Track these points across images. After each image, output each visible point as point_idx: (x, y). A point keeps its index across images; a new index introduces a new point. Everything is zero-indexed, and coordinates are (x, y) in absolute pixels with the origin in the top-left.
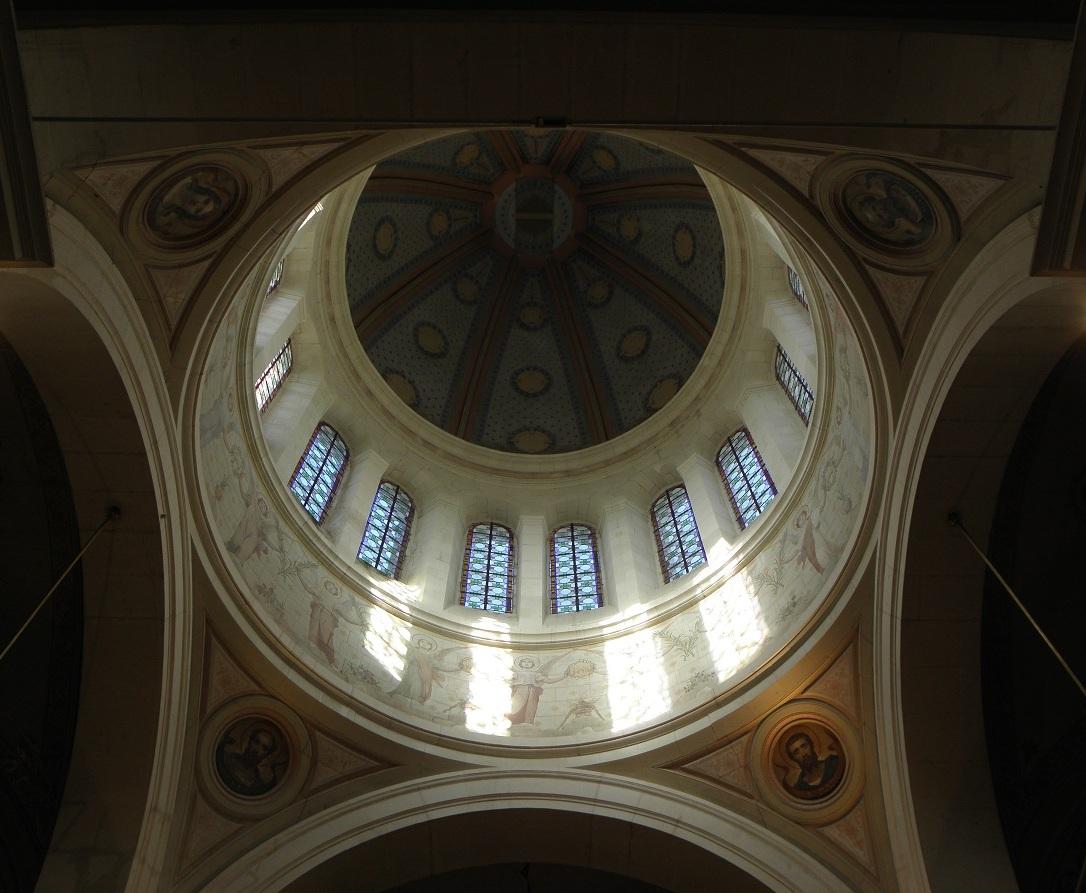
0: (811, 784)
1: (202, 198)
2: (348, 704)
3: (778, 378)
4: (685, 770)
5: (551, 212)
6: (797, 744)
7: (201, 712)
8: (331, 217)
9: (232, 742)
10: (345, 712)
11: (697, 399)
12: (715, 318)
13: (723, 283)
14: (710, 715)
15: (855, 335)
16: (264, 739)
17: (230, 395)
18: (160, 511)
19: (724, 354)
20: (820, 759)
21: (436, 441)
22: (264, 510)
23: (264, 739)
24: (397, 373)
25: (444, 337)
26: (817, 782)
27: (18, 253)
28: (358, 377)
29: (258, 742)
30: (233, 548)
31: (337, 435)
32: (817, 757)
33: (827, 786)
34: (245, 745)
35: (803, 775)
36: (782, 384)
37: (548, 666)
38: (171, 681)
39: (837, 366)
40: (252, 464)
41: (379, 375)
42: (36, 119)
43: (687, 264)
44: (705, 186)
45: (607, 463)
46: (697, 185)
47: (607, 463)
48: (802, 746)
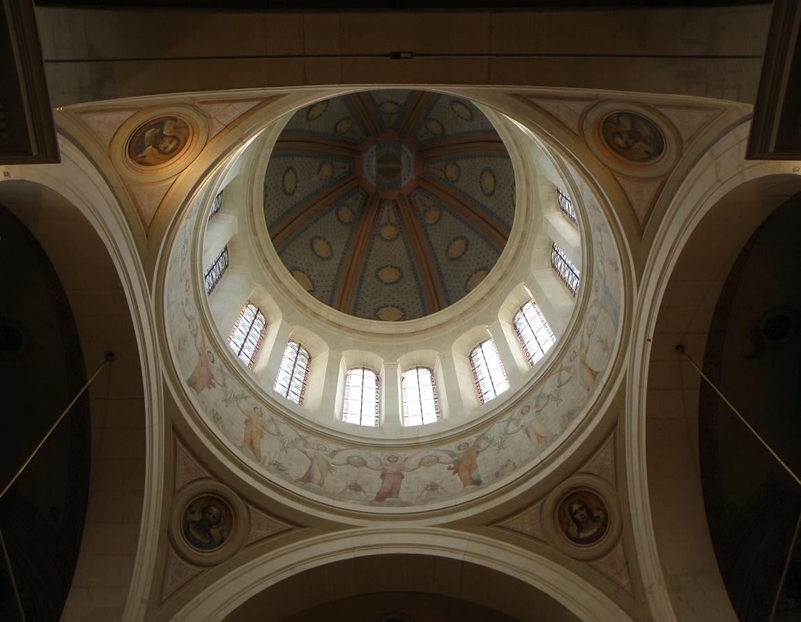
1: (578, 516)
3: (553, 266)
4: (583, 473)
5: (400, 163)
7: (171, 489)
8: (252, 157)
9: (646, 152)
12: (510, 229)
13: (514, 206)
14: (469, 510)
15: (613, 237)
18: (650, 345)
22: (212, 358)
23: (215, 510)
24: (299, 270)
26: (148, 134)
27: (35, 153)
30: (191, 383)
31: (259, 310)
33: (139, 135)
35: (162, 131)
36: (556, 269)
37: (335, 452)
39: (595, 253)
41: (287, 271)
42: (48, 61)
43: (491, 194)
44: (502, 142)
46: (504, 237)
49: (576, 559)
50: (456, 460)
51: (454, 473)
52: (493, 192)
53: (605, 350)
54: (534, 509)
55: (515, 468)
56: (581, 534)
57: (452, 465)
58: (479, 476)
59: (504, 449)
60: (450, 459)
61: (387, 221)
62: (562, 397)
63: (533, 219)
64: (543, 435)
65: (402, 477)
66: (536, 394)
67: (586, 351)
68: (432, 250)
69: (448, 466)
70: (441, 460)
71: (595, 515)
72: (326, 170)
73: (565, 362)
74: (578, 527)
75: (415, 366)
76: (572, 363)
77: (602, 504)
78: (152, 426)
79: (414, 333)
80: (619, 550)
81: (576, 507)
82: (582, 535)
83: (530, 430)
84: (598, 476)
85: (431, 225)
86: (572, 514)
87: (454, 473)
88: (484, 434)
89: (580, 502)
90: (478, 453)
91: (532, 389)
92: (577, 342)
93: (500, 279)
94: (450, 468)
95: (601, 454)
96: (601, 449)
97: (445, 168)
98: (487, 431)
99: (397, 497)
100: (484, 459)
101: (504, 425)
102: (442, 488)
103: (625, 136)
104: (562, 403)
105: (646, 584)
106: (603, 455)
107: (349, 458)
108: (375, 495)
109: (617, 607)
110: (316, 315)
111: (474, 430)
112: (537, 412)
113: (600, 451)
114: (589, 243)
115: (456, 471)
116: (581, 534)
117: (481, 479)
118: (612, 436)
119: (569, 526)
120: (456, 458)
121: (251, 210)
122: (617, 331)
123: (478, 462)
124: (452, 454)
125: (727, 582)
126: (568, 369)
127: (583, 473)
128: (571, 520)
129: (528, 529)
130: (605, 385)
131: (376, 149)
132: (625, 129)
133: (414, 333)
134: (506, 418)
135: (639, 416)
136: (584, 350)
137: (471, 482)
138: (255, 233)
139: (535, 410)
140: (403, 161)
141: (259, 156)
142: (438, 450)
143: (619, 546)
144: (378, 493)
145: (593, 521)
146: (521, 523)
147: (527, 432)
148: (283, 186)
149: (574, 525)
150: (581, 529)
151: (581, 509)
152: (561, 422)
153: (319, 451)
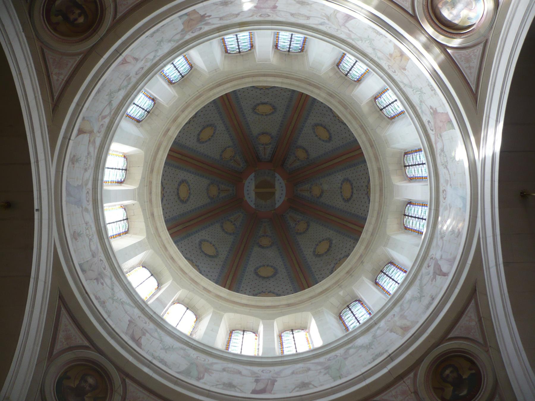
0: (460, 395)
1: (78, 11)
2: (148, 367)
4: (124, 382)
6: (448, 372)
9: (69, 378)
10: (146, 370)
11: (361, 256)
16: (91, 380)
17: (88, 192)
18: (36, 207)
19: (374, 229)
20: (464, 377)
21: (211, 289)
23: (91, 380)
25: (216, 249)
26: (464, 393)
28: (166, 249)
29: (86, 381)
32: (462, 377)
34: (77, 382)
38: (32, 312)
40: (98, 241)
45: (312, 298)
47: (312, 298)
48: (451, 372)
51: (206, 14)
52: (179, 185)
60: (210, 21)
61: (267, 147)
63: (146, 187)
67: (90, 141)
68: (227, 129)
69: (210, 18)
70: (218, 19)
72: (316, 191)
73: (107, 120)
75: (241, 54)
76: (102, 123)
77: (55, 30)
78: (496, 265)
79: (243, 78)
81: (81, 20)
85: (229, 147)
87: (206, 14)
88: (177, 42)
90: (182, 30)
92: (98, 141)
93: (169, 130)
94: (209, 16)
96: (64, 82)
97: (219, 193)
101: (158, 54)
103: (88, 388)
106: (62, 77)
107: (307, 19)
110: (331, 95)
111: (187, 43)
112: (128, 76)
114: (99, 230)
121: (381, 190)
124: (207, 24)
127: (124, 382)
128: (84, 6)
130: (70, 139)
131: (275, 204)
132: (89, 395)
133: (243, 78)
135: (33, 133)
136: (92, 141)
138: (379, 170)
139: (130, 76)
140: (253, 195)
141: (372, 235)
147: (136, 60)
148: (352, 189)
149: (80, 3)
151: (76, 20)
153: (337, 28)
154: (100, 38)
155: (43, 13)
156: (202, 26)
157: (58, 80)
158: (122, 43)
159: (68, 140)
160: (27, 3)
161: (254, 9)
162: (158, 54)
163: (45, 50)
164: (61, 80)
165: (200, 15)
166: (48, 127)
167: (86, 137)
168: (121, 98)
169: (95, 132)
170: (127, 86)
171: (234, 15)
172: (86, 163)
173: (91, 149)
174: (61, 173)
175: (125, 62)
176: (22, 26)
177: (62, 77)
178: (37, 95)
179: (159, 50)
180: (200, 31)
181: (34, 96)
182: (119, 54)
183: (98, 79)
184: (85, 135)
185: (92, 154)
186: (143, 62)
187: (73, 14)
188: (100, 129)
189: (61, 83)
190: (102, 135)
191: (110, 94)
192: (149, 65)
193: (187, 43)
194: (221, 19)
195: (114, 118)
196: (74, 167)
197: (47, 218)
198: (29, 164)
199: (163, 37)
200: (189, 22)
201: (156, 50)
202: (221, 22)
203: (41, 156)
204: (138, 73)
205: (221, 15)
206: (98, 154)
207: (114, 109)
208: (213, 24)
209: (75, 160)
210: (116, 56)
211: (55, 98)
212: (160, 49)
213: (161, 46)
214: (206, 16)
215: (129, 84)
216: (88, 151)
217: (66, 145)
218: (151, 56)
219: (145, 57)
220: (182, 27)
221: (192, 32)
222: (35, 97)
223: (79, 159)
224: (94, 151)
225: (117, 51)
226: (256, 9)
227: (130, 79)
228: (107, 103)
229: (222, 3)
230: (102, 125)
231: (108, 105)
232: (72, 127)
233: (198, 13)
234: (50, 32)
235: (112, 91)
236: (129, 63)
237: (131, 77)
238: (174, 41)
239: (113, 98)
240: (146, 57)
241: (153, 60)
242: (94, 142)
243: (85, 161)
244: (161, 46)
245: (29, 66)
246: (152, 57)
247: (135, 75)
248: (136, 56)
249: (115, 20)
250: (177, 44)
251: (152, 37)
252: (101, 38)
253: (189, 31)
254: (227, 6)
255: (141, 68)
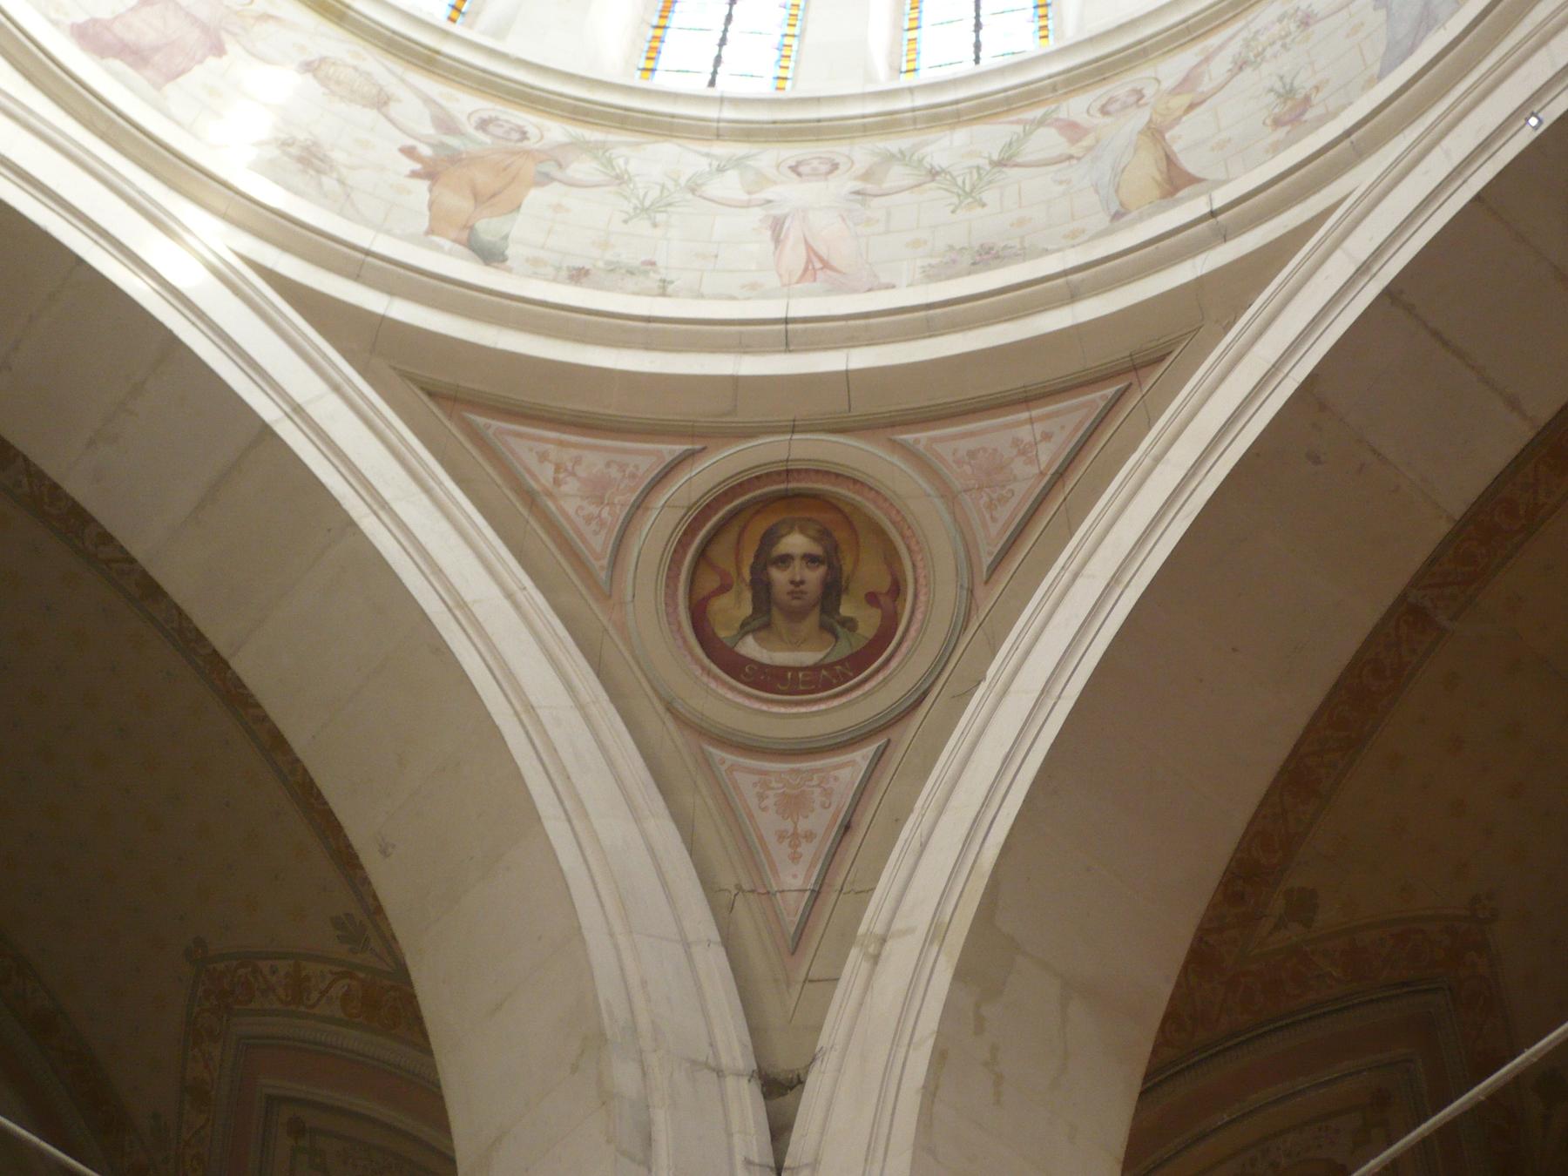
1: (779, 577)
4: (909, 452)
49: (670, 708)
50: (442, 145)
51: (414, 174)
53: (1277, 123)
54: (648, 456)
55: (663, 290)
56: (750, 640)
57: (425, 151)
58: (506, 237)
59: (655, 225)
60: (428, 130)
62: (989, 196)
64: (835, 261)
65: (219, 50)
66: (894, 144)
67: (1192, 107)
69: (410, 142)
70: (394, 110)
71: (846, 610)
73: (1077, 107)
74: (756, 609)
76: (1100, 120)
77: (897, 589)
80: (851, 767)
82: (750, 648)
83: (793, 232)
84: (949, 495)
86: (767, 558)
87: (414, 174)
88: (603, 146)
89: (823, 535)
90: (545, 179)
91: (888, 124)
92: (1172, 68)
94: (409, 152)
95: (1021, 426)
96: (1035, 413)
98: (627, 144)
99: (158, 87)
100: (558, 208)
101: (703, 164)
102: (341, 182)
104: (979, 211)
105: (873, 919)
106: (1025, 433)
108: (81, 18)
109: (715, 935)
111: (578, 112)
112: (857, 193)
113: (1025, 415)
115: (430, 173)
116: (750, 640)
117: (509, 252)
118: (1110, 391)
119: (724, 589)
120: (453, 141)
122: (1381, 77)
123: (526, 202)
124: (446, 124)
125: (1154, 1082)
126: (1072, 130)
127: (909, 452)
129: (571, 503)
130: (1213, 214)
134: (723, 149)
136: (1185, 100)
137: (465, 235)
139: (859, 185)
142: (402, 80)
143: (861, 757)
144: (95, 21)
145: (825, 627)
146: (558, 468)
147: (777, 228)
150: (761, 620)
151: (810, 559)
152: (933, 261)
154: (796, 437)
155: (877, 671)
156: (471, 130)
157: (1047, 436)
158: (746, 353)
159: (1221, 218)
160: (889, 741)
161: (230, 45)
162: (703, 164)
163: (987, 561)
164: (1039, 428)
165: (430, 190)
166: (1227, 329)
167: (1187, 140)
168: (960, 136)
169: (1147, 119)
170: (901, 157)
171: (324, 81)
172: (1279, 43)
173: (1220, 67)
174: (1353, 137)
175: (815, 260)
176: (970, 693)
177: (1025, 433)
178: (1148, 461)
179: (683, 181)
180: (493, 114)
181: (1160, 467)
182: (790, 326)
183: (931, 312)
184: (1176, 148)
185: (1235, 47)
186: (769, 193)
187: (802, 582)
188: (1125, 107)
189: (1049, 416)
190: (1140, 76)
191: (969, 194)
192: (769, 157)
193: (578, 112)
194: (381, 102)
195: (1054, 88)
196: (1317, 88)
197: (1542, 54)
198: (1390, 294)
199: (626, 222)
200: (493, 196)
201: (693, 191)
202: (392, 86)
203: (1338, 269)
204: (824, 168)
205: (371, 115)
206: (1225, 22)
207: (1018, 122)
208: (428, 100)
209: (1290, 103)
210: (805, 331)
211: (1110, 391)
212: (676, 181)
213: (663, 187)
214: (417, 166)
215: (890, 158)
216: (1232, 77)
217: (1244, 205)
218: (730, 185)
219: (748, 205)
220: (536, 199)
221: (524, 135)
222: (1158, 460)
223: (1278, 85)
224: (1221, 47)
225: (787, 344)
226: (225, 37)
227: (867, 176)
228: (1012, 173)
229: (319, 171)
230: (1104, 111)
231: (1019, 160)
232: (1161, 244)
233: (431, 205)
234: (916, 596)
235: (955, 200)
236: (809, 247)
237: (857, 178)
238: (610, 163)
239: (978, 168)
240: (745, 197)
241: (739, 163)
242: (1188, 81)
243: (1275, 56)
244: (663, 187)
245: (1074, 567)
246: (732, 175)
247: (842, 168)
248: (762, 245)
249: (698, 447)
250: (614, 137)
251: (653, 264)
252: (793, 432)
253: (528, 153)
254: (315, 144)
255: (799, 174)
